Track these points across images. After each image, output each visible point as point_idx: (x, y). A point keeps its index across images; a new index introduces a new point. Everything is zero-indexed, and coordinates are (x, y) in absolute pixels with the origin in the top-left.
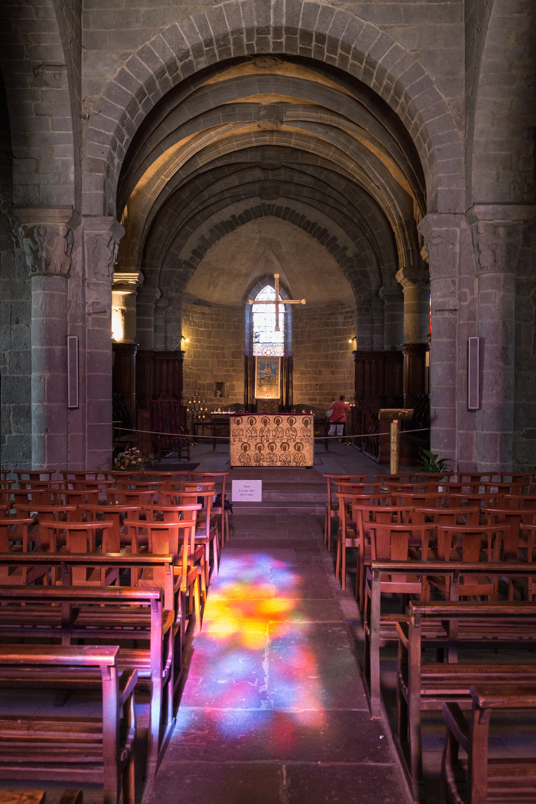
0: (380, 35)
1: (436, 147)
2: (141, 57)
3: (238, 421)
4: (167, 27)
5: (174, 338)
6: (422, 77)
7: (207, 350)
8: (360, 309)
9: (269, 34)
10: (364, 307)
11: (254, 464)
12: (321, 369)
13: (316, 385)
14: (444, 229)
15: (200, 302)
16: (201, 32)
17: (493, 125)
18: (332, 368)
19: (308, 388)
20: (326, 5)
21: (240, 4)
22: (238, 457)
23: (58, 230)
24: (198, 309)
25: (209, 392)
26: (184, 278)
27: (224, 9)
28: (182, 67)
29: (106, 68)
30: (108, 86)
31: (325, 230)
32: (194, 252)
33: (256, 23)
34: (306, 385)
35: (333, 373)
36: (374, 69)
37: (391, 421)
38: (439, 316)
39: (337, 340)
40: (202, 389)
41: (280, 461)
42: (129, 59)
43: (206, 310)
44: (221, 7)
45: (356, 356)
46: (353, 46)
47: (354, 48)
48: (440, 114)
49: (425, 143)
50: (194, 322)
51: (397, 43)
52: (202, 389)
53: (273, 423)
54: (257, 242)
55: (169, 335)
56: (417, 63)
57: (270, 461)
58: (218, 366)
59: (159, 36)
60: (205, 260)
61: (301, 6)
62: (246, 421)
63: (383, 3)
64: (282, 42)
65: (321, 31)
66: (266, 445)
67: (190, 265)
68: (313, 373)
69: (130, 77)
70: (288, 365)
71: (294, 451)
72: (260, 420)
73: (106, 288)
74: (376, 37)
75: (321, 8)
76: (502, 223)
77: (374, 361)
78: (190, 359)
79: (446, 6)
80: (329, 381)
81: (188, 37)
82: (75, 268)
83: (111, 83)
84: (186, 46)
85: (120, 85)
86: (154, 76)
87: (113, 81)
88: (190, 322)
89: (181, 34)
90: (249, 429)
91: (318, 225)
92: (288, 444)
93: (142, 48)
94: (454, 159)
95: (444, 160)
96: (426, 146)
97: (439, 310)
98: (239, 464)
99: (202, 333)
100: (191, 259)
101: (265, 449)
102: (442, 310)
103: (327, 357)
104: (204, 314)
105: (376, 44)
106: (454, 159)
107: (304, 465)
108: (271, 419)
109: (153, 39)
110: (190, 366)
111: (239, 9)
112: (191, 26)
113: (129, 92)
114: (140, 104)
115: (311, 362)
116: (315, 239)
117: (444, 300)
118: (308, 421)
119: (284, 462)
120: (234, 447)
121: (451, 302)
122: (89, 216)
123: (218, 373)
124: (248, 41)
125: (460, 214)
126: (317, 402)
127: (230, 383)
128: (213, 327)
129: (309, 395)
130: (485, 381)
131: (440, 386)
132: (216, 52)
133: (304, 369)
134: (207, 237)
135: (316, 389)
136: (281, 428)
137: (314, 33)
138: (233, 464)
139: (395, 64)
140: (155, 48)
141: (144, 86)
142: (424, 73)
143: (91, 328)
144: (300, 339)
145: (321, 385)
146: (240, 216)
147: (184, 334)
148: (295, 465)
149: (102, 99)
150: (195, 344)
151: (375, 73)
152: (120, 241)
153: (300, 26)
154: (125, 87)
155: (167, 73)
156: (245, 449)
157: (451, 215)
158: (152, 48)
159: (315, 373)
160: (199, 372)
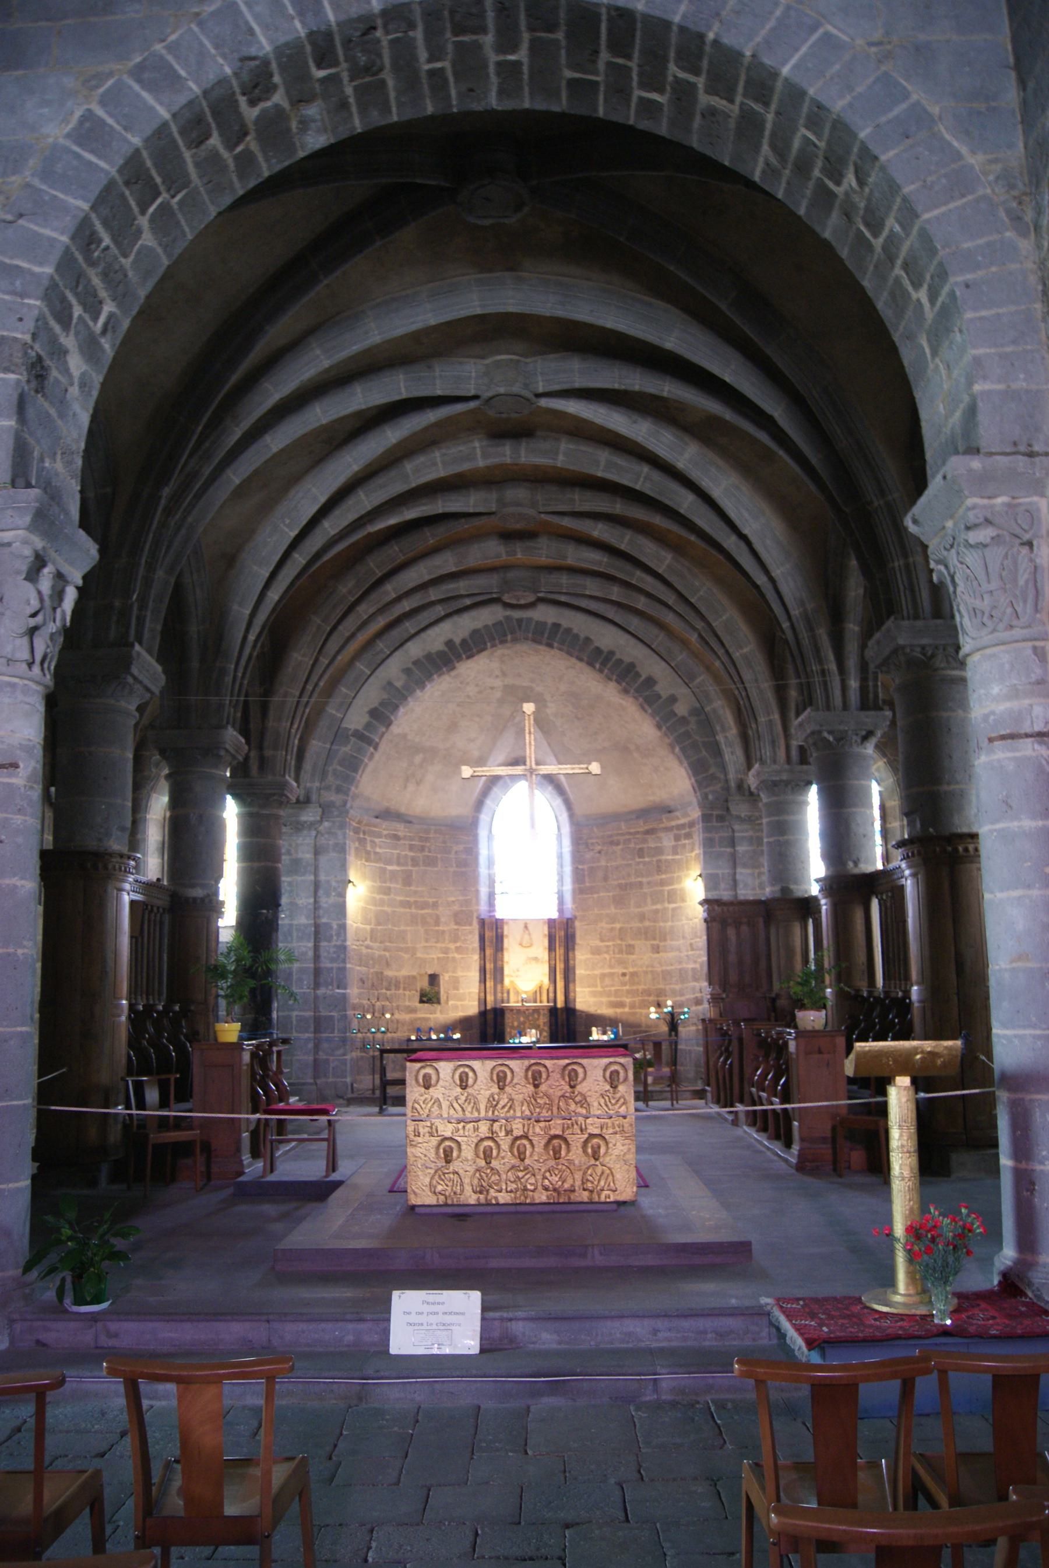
1: (959, 279)
2: (139, 81)
3: (427, 1078)
4: (213, 8)
5: (334, 884)
6: (904, 106)
7: (402, 910)
8: (706, 818)
9: (483, 30)
10: (715, 813)
11: (472, 1199)
12: (632, 942)
13: (624, 975)
14: (999, 500)
15: (387, 815)
16: (301, 13)
18: (654, 939)
19: (607, 981)
22: (427, 1180)
24: (385, 827)
25: (407, 993)
26: (353, 765)
29: (46, 110)
31: (632, 665)
32: (374, 713)
34: (603, 976)
35: (656, 949)
36: (766, 104)
37: (888, 1081)
38: (1001, 754)
39: (662, 883)
40: (393, 987)
41: (546, 1189)
43: (401, 829)
45: (709, 911)
48: (963, 196)
49: (917, 286)
50: (375, 853)
51: (830, 28)
52: (393, 987)
53: (523, 1082)
54: (498, 694)
55: (322, 877)
56: (886, 74)
57: (517, 1190)
58: (427, 941)
59: (190, 29)
60: (395, 729)
62: (449, 1078)
64: (517, 64)
66: (505, 1145)
67: (365, 739)
68: (616, 950)
69: (107, 129)
70: (567, 936)
71: (584, 1159)
72: (487, 1075)
73: (20, 697)
74: (771, 13)
78: (368, 927)
80: (648, 966)
81: (265, 27)
84: (262, 48)
86: (174, 129)
88: (368, 853)
89: (247, 23)
90: (457, 1098)
91: (618, 656)
92: (565, 1140)
93: (145, 59)
95: (984, 313)
96: (922, 295)
97: (1003, 738)
98: (431, 1200)
99: (393, 876)
100: (368, 726)
101: (502, 1154)
102: (1012, 736)
103: (642, 917)
104: (396, 837)
105: (773, 29)
107: (612, 1199)
108: (516, 1069)
109: (173, 37)
110: (368, 942)
113: (102, 164)
114: (143, 212)
115: (612, 930)
116: (612, 685)
117: (1014, 705)
118: (617, 1072)
119: (555, 1190)
121: (1038, 710)
123: (426, 956)
124: (430, 61)
126: (627, 1010)
127: (450, 974)
128: (415, 862)
129: (609, 994)
131: (1020, 964)
132: (349, 90)
133: (598, 943)
134: (398, 684)
135: (624, 984)
136: (546, 1095)
137: (604, 11)
138: (414, 1200)
139: (828, 75)
140: (177, 57)
141: (145, 154)
142: (906, 96)
144: (587, 884)
145: (633, 974)
146: (464, 642)
147: (352, 875)
148: (586, 1200)
149: (28, 186)
150: (378, 897)
151: (770, 117)
152: (85, 578)
154: (92, 151)
155: (215, 134)
156: (448, 1158)
157: (1020, 457)
158: (170, 58)
159: (621, 952)
160: (387, 954)
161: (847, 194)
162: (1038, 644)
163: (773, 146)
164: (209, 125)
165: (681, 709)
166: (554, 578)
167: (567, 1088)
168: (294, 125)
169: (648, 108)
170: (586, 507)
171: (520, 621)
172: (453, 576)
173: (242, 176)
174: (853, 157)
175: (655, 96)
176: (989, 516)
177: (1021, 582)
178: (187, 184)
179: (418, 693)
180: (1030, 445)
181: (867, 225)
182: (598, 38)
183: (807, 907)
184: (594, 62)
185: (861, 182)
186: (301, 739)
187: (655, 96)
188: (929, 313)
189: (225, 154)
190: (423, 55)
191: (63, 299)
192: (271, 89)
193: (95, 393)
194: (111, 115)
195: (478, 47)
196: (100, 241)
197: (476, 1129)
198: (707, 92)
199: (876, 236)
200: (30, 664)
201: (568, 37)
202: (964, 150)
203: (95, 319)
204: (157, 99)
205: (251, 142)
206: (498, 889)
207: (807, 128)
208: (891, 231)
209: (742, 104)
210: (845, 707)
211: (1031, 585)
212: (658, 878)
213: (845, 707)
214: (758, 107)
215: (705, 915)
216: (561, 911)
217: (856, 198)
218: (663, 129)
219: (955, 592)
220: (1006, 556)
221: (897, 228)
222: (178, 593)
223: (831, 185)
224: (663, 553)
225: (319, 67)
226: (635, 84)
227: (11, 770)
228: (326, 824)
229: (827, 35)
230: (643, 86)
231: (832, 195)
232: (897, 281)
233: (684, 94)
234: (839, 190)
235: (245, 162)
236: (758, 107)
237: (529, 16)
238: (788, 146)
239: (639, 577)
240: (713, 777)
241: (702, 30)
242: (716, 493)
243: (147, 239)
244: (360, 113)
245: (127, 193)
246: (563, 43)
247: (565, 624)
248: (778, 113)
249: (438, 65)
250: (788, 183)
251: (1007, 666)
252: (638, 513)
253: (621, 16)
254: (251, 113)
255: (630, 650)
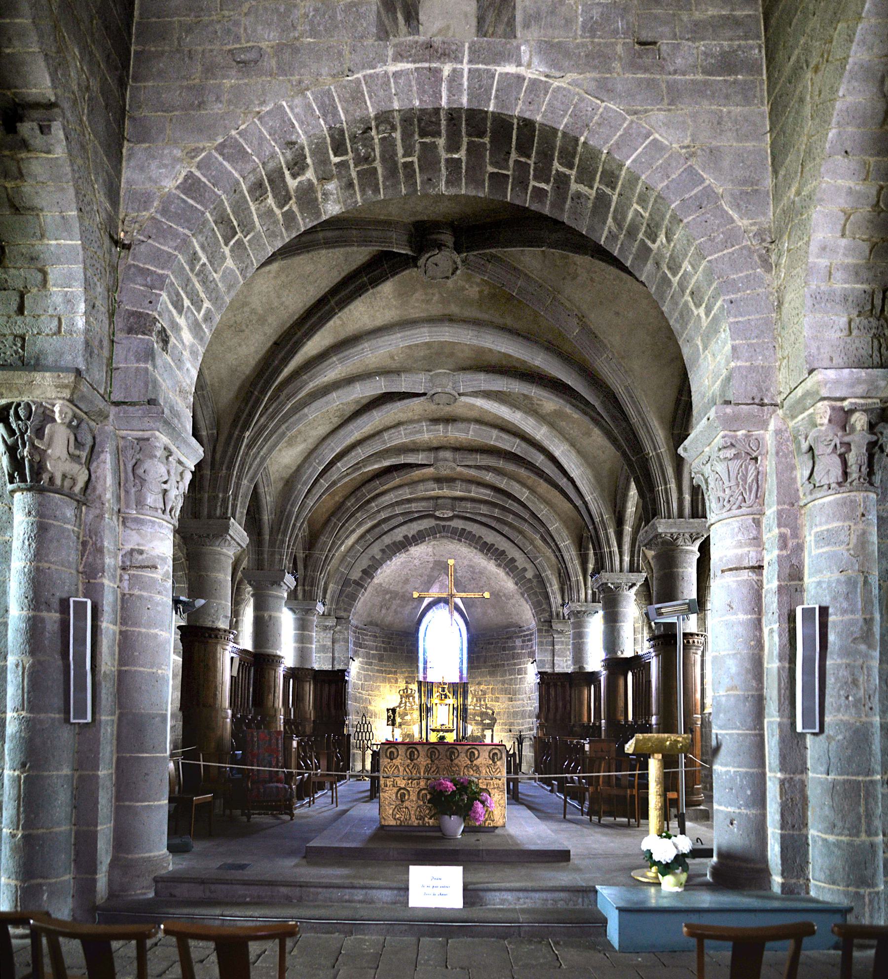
0: (627, 122)
2: (221, 154)
6: (700, 188)
8: (540, 631)
9: (438, 134)
14: (740, 433)
16: (325, 116)
17: (843, 235)
20: (535, 76)
21: (391, 75)
22: (391, 812)
23: (53, 412)
27: (363, 82)
28: (297, 189)
30: (165, 198)
32: (365, 572)
33: (417, 103)
36: (614, 189)
39: (515, 664)
42: (201, 157)
44: (358, 78)
46: (582, 139)
47: (585, 143)
49: (698, 306)
55: (336, 655)
56: (691, 166)
59: (254, 122)
61: (493, 78)
63: (631, 76)
64: (459, 160)
65: (527, 115)
74: (621, 125)
75: (526, 81)
76: (862, 405)
77: (559, 684)
79: (735, 82)
81: (302, 123)
82: (94, 489)
83: (169, 193)
85: (184, 197)
87: (174, 191)
89: (290, 119)
90: (408, 766)
94: (757, 316)
96: (702, 311)
97: (731, 570)
99: (374, 656)
100: (361, 578)
102: (736, 569)
105: (621, 136)
106: (757, 316)
108: (441, 751)
111: (389, 80)
112: (309, 106)
113: (199, 207)
114: (226, 244)
117: (740, 551)
120: (386, 795)
122: (124, 403)
124: (404, 156)
125: (772, 405)
128: (385, 650)
130: (830, 681)
134: (378, 557)
137: (515, 121)
143: (126, 591)
149: (153, 218)
151: (615, 198)
153: (491, 109)
154: (192, 198)
158: (241, 140)
161: (659, 248)
162: (756, 516)
163: (615, 219)
164: (266, 188)
165: (529, 575)
166: (463, 504)
167: (469, 762)
168: (319, 195)
169: (539, 194)
170: (483, 463)
171: (444, 527)
172: (409, 501)
173: (287, 228)
174: (666, 222)
175: (543, 186)
176: (733, 442)
177: (749, 480)
178: (253, 228)
179: (388, 562)
180: (762, 399)
181: (669, 268)
182: (511, 143)
183: (592, 677)
184: (507, 160)
185: (669, 240)
186: (325, 583)
187: (543, 186)
188: (705, 322)
189: (277, 211)
190: (400, 151)
191: (178, 294)
192: (303, 168)
193: (200, 359)
194: (205, 176)
195: (434, 146)
196: (200, 259)
197: (418, 784)
198: (576, 181)
199: (674, 275)
200: (164, 512)
201: (491, 142)
202: (736, 216)
203: (199, 311)
204: (234, 168)
205: (293, 205)
206: (429, 665)
207: (637, 203)
208: (685, 270)
209: (598, 188)
210: (621, 570)
211: (755, 484)
212: (512, 662)
213: (621, 570)
214: (608, 191)
215: (538, 680)
216: (461, 678)
217: (665, 251)
218: (546, 211)
219: (707, 489)
220: (741, 466)
221: (689, 268)
222: (255, 495)
223: (649, 243)
224: (524, 490)
225: (335, 156)
226: (531, 177)
227: (153, 570)
228: (338, 627)
229: (655, 140)
230: (536, 178)
231: (649, 250)
232: (686, 304)
233: (562, 182)
234: (654, 247)
235: (289, 217)
236: (608, 191)
237: (467, 125)
238: (624, 218)
239: (509, 504)
240: (544, 610)
241: (577, 135)
242: (557, 454)
243: (229, 263)
244: (360, 191)
245: (216, 229)
246: (488, 146)
247: (468, 529)
248: (620, 195)
249: (410, 159)
250: (622, 245)
251: (736, 530)
252: (511, 467)
253: (526, 125)
254: (292, 184)
255: (502, 544)
